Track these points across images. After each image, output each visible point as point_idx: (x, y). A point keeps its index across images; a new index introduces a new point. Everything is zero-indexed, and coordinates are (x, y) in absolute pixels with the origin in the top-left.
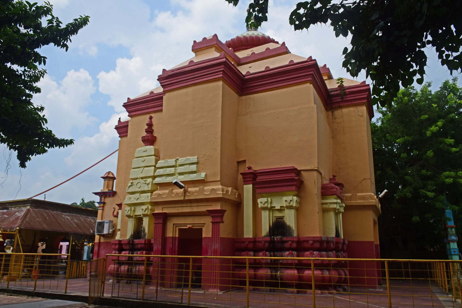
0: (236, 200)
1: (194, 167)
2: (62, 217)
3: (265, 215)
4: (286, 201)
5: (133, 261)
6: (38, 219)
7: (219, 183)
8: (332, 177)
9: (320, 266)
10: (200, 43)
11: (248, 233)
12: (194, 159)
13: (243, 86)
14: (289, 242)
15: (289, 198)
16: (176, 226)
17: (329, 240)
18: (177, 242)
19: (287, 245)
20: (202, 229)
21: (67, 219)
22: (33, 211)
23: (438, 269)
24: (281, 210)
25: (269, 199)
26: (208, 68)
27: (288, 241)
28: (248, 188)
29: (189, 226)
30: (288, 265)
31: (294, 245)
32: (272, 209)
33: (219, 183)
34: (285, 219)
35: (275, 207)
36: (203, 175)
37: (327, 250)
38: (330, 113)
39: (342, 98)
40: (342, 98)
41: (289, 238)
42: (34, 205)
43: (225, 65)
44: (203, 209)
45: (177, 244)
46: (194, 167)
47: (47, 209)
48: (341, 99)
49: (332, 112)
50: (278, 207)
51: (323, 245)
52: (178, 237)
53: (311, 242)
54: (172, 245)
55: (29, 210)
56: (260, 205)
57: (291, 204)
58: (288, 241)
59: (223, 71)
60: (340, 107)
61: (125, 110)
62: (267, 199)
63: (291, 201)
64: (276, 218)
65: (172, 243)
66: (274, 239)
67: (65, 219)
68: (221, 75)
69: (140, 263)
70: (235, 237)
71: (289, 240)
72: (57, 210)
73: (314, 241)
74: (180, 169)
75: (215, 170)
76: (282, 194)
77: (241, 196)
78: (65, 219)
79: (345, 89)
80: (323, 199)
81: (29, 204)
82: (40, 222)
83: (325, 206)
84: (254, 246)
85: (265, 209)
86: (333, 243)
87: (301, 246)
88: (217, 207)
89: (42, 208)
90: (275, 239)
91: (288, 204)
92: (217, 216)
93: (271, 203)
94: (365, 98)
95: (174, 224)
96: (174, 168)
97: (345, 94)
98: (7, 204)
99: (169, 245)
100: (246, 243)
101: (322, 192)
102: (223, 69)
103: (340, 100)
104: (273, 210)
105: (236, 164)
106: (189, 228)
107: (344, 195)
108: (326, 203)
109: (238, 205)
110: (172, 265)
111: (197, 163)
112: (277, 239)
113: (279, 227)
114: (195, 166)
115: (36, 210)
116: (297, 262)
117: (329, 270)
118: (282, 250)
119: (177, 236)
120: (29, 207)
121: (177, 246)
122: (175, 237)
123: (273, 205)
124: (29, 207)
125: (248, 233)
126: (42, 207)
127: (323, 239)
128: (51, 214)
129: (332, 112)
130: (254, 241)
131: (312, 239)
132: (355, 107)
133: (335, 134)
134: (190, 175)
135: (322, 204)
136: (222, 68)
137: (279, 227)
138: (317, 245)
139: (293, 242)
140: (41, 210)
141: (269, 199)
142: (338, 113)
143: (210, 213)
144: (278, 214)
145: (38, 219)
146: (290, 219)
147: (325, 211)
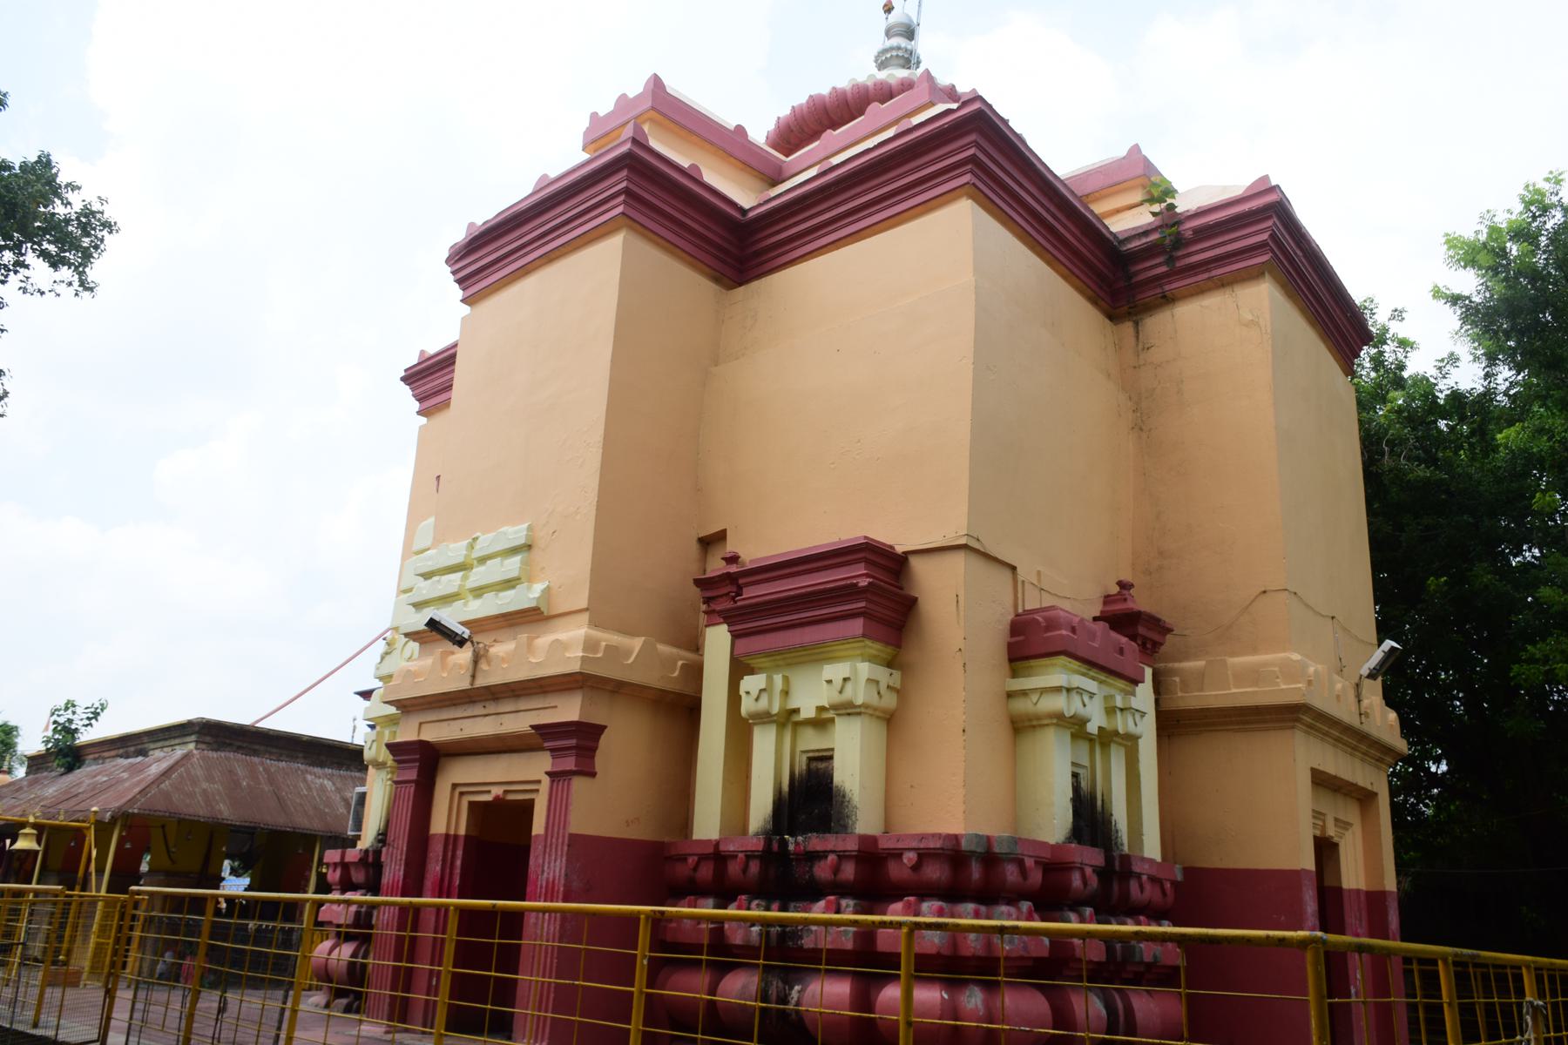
0: (676, 687)
1: (513, 565)
2: (305, 780)
3: (764, 743)
4: (829, 682)
5: (371, 927)
6: (205, 785)
7: (585, 617)
8: (1115, 589)
9: (949, 967)
10: (609, 115)
11: (707, 824)
12: (515, 533)
13: (738, 248)
14: (832, 857)
15: (835, 671)
16: (462, 794)
17: (997, 849)
18: (460, 853)
19: (822, 871)
20: (532, 801)
21: (323, 788)
22: (204, 758)
23: (787, 956)
24: (821, 723)
25: (778, 679)
26: (581, 191)
27: (822, 855)
28: (718, 640)
29: (497, 791)
30: (723, 954)
31: (849, 871)
32: (787, 719)
33: (585, 617)
34: (837, 762)
35: (796, 711)
36: (537, 589)
37: (989, 895)
38: (1128, 327)
39: (1171, 260)
40: (1171, 260)
41: (831, 842)
42: (208, 739)
43: (632, 168)
44: (517, 720)
45: (458, 863)
46: (513, 565)
47: (255, 753)
48: (1166, 263)
49: (1137, 324)
50: (808, 712)
51: (967, 872)
52: (466, 836)
53: (910, 858)
54: (443, 869)
55: (186, 757)
56: (747, 706)
57: (848, 693)
58: (822, 855)
59: (626, 191)
60: (1168, 300)
61: (410, 392)
62: (770, 680)
63: (845, 680)
64: (810, 759)
65: (444, 860)
66: (784, 844)
67: (309, 789)
68: (620, 209)
69: (723, 954)
70: (666, 839)
71: (830, 847)
72: (292, 758)
73: (924, 856)
74: (479, 575)
75: (565, 575)
76: (815, 655)
77: (695, 672)
78: (309, 789)
79: (1178, 223)
80: (1015, 674)
81: (193, 738)
82: (212, 792)
83: (1022, 706)
84: (718, 875)
85: (764, 718)
86: (1020, 863)
87: (874, 874)
88: (568, 710)
89: (239, 749)
90: (791, 847)
91: (837, 698)
92: (577, 745)
93: (786, 693)
94: (1261, 246)
95: (455, 786)
96: (460, 574)
97: (1179, 242)
98: (145, 739)
99: (434, 868)
100: (690, 860)
101: (1010, 646)
102: (624, 184)
103: (1164, 269)
104: (798, 724)
105: (694, 548)
106: (497, 798)
107: (1177, 665)
108: (1024, 693)
109: (681, 709)
110: (400, 940)
111: (528, 547)
112: (797, 844)
113: (811, 796)
114: (516, 560)
115: (215, 755)
116: (1097, 953)
117: (990, 987)
118: (811, 892)
119: (462, 831)
120: (192, 746)
121: (458, 871)
122: (456, 837)
123: (792, 705)
124: (192, 746)
125: (707, 824)
126: (239, 748)
127: (964, 845)
128: (267, 770)
129: (1137, 324)
130: (717, 855)
131: (914, 844)
132: (1228, 291)
133: (1144, 411)
134: (502, 594)
135: (1010, 695)
136: (620, 181)
137: (811, 796)
138: (935, 872)
139: (843, 856)
140: (231, 755)
141: (778, 679)
142: (1159, 324)
143: (546, 733)
144: (812, 741)
145: (205, 785)
146: (853, 761)
147: (1021, 727)
